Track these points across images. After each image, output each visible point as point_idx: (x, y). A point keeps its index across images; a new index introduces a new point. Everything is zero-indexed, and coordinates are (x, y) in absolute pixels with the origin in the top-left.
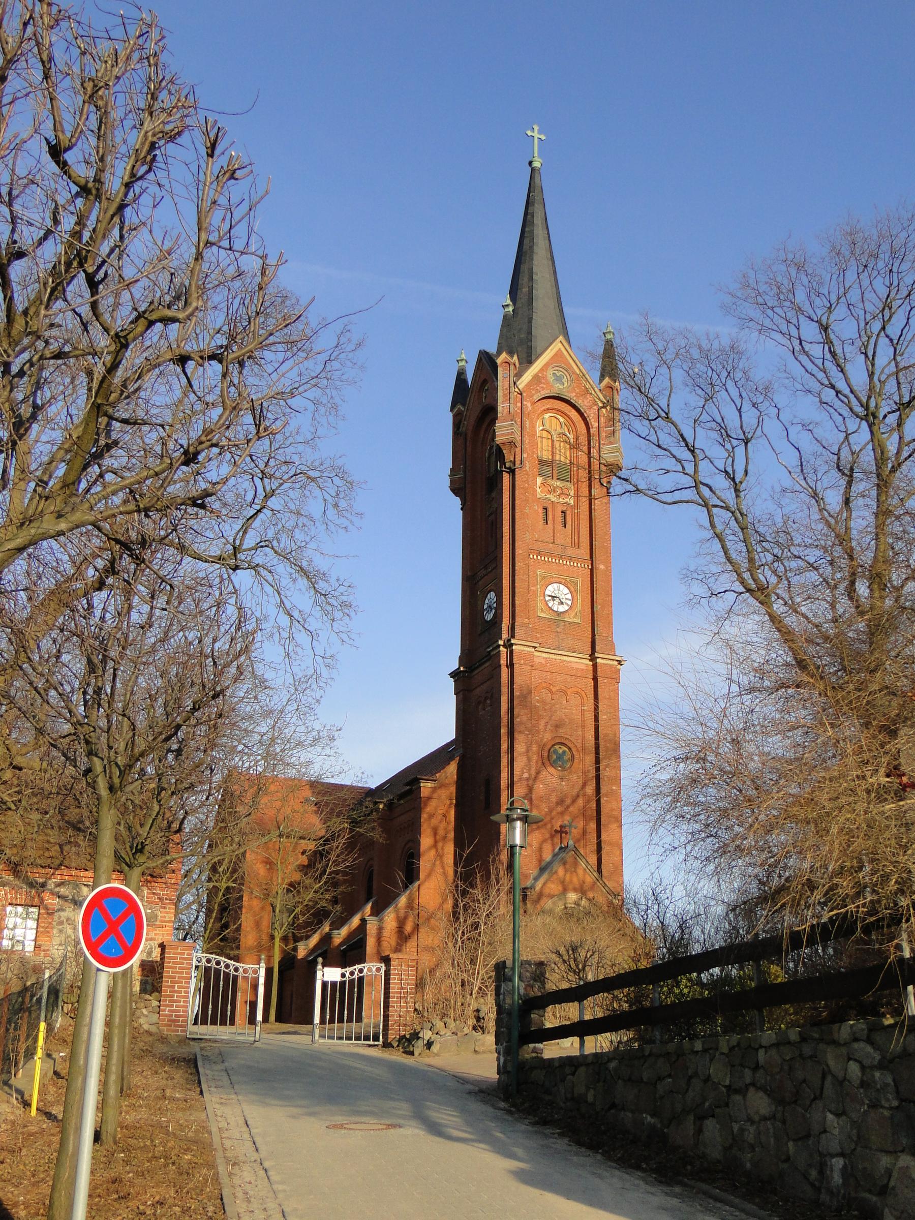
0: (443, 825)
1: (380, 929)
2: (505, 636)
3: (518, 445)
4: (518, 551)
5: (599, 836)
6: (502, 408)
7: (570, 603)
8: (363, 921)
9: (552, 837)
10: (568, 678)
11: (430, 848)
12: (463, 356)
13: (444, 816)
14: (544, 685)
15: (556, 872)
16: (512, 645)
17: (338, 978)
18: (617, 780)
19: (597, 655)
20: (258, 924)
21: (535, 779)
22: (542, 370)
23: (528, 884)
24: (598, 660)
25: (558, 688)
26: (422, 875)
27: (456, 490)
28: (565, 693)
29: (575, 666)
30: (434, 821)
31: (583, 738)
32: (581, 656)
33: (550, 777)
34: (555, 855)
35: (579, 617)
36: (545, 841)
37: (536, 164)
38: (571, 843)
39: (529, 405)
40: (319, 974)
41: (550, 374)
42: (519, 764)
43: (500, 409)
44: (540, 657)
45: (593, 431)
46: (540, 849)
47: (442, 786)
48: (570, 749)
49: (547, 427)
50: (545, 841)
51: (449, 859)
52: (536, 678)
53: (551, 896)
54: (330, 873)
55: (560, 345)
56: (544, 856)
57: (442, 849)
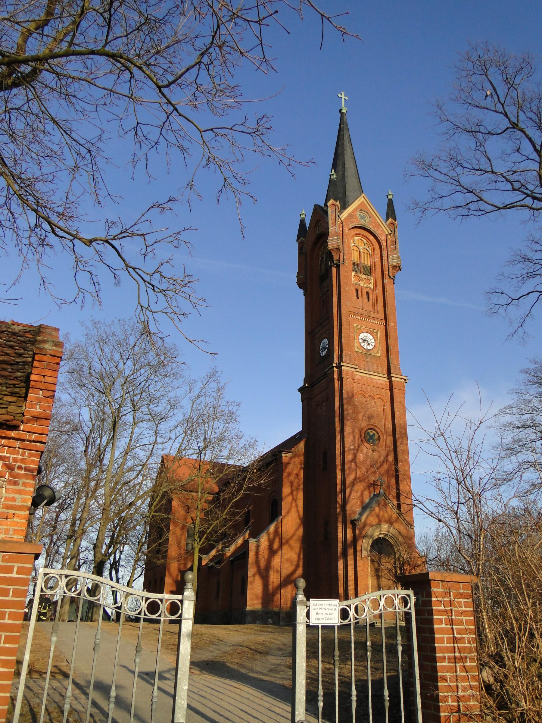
0: (297, 480)
1: (258, 547)
2: (336, 361)
3: (341, 251)
4: (343, 312)
5: (398, 489)
6: (331, 229)
7: (373, 344)
8: (246, 543)
9: (369, 487)
10: (374, 388)
11: (288, 495)
12: (303, 212)
13: (297, 475)
14: (361, 392)
15: (374, 510)
16: (341, 366)
17: (335, 620)
18: (406, 452)
19: (392, 375)
20: (178, 543)
21: (358, 450)
22: (353, 211)
23: (356, 517)
24: (393, 379)
25: (369, 394)
26: (284, 512)
27: (301, 284)
28: (374, 398)
29: (378, 382)
30: (292, 478)
31: (385, 426)
32: (382, 375)
33: (366, 450)
34: (371, 499)
35: (381, 352)
36: (364, 490)
37: (344, 111)
38: (382, 491)
39: (347, 229)
40: (301, 612)
41: (358, 213)
42: (348, 440)
43: (330, 230)
44: (358, 375)
45: (384, 247)
46: (362, 495)
47: (296, 456)
48: (377, 433)
49: (356, 244)
50: (364, 490)
51: (300, 503)
52: (357, 388)
53: (372, 526)
54: (248, 489)
55: (363, 199)
56: (364, 499)
57: (296, 496)
